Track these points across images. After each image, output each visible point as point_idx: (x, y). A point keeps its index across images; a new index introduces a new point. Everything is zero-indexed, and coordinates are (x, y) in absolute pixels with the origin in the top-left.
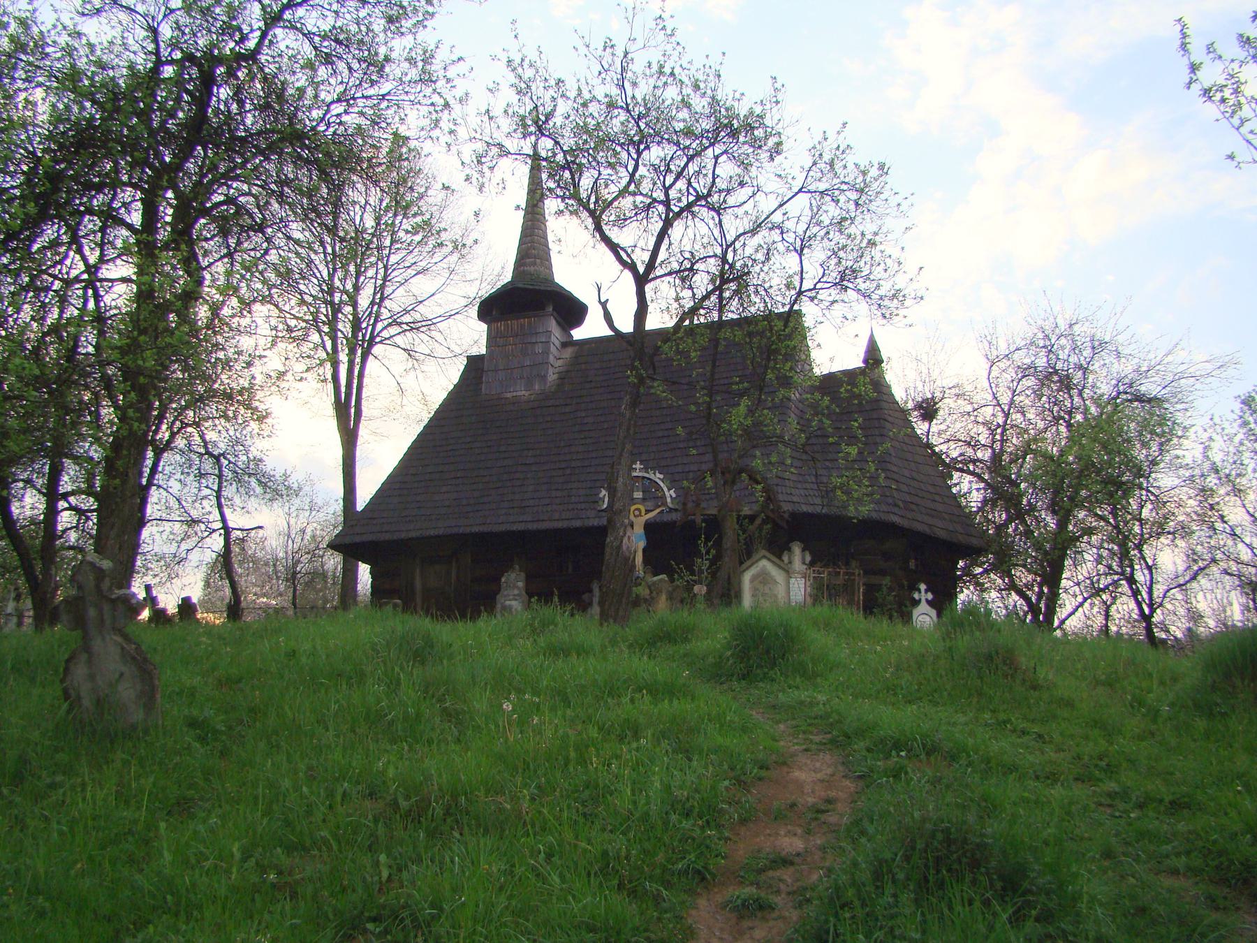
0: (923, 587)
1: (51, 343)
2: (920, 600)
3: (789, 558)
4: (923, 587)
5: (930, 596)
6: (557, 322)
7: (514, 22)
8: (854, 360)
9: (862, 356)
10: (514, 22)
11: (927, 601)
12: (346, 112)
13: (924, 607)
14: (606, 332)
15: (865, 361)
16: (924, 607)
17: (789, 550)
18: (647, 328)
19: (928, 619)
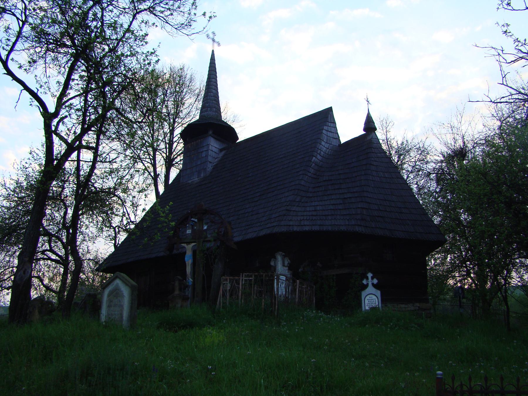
0: (370, 275)
1: (10, 248)
2: (368, 284)
3: (275, 263)
4: (370, 275)
5: (375, 281)
6: (215, 138)
7: (160, 43)
8: (359, 131)
9: (363, 126)
10: (160, 43)
11: (373, 284)
12: (126, 128)
13: (370, 289)
14: (36, 92)
15: (365, 130)
16: (370, 289)
17: (275, 258)
18: (342, 143)
19: (374, 297)
